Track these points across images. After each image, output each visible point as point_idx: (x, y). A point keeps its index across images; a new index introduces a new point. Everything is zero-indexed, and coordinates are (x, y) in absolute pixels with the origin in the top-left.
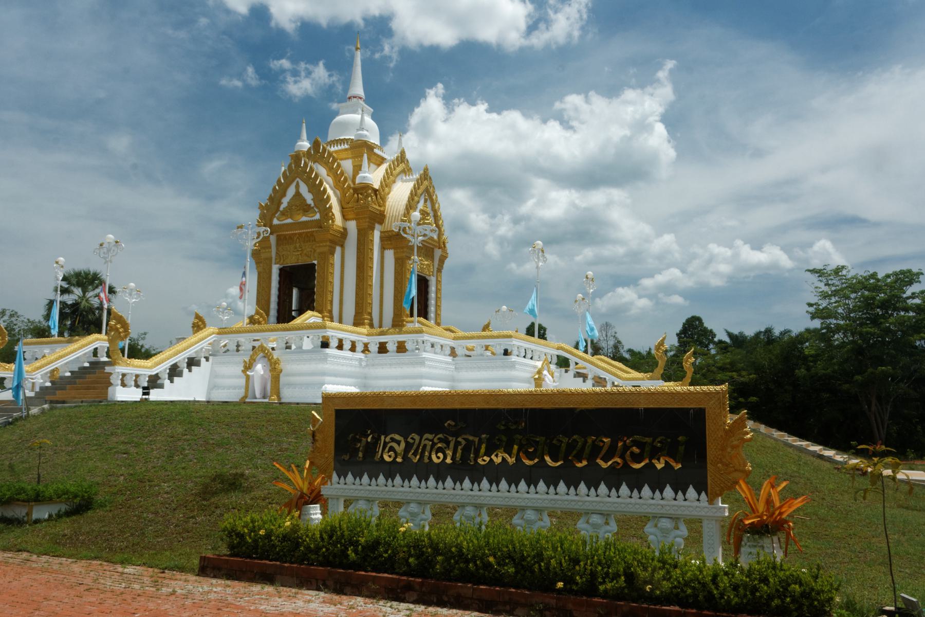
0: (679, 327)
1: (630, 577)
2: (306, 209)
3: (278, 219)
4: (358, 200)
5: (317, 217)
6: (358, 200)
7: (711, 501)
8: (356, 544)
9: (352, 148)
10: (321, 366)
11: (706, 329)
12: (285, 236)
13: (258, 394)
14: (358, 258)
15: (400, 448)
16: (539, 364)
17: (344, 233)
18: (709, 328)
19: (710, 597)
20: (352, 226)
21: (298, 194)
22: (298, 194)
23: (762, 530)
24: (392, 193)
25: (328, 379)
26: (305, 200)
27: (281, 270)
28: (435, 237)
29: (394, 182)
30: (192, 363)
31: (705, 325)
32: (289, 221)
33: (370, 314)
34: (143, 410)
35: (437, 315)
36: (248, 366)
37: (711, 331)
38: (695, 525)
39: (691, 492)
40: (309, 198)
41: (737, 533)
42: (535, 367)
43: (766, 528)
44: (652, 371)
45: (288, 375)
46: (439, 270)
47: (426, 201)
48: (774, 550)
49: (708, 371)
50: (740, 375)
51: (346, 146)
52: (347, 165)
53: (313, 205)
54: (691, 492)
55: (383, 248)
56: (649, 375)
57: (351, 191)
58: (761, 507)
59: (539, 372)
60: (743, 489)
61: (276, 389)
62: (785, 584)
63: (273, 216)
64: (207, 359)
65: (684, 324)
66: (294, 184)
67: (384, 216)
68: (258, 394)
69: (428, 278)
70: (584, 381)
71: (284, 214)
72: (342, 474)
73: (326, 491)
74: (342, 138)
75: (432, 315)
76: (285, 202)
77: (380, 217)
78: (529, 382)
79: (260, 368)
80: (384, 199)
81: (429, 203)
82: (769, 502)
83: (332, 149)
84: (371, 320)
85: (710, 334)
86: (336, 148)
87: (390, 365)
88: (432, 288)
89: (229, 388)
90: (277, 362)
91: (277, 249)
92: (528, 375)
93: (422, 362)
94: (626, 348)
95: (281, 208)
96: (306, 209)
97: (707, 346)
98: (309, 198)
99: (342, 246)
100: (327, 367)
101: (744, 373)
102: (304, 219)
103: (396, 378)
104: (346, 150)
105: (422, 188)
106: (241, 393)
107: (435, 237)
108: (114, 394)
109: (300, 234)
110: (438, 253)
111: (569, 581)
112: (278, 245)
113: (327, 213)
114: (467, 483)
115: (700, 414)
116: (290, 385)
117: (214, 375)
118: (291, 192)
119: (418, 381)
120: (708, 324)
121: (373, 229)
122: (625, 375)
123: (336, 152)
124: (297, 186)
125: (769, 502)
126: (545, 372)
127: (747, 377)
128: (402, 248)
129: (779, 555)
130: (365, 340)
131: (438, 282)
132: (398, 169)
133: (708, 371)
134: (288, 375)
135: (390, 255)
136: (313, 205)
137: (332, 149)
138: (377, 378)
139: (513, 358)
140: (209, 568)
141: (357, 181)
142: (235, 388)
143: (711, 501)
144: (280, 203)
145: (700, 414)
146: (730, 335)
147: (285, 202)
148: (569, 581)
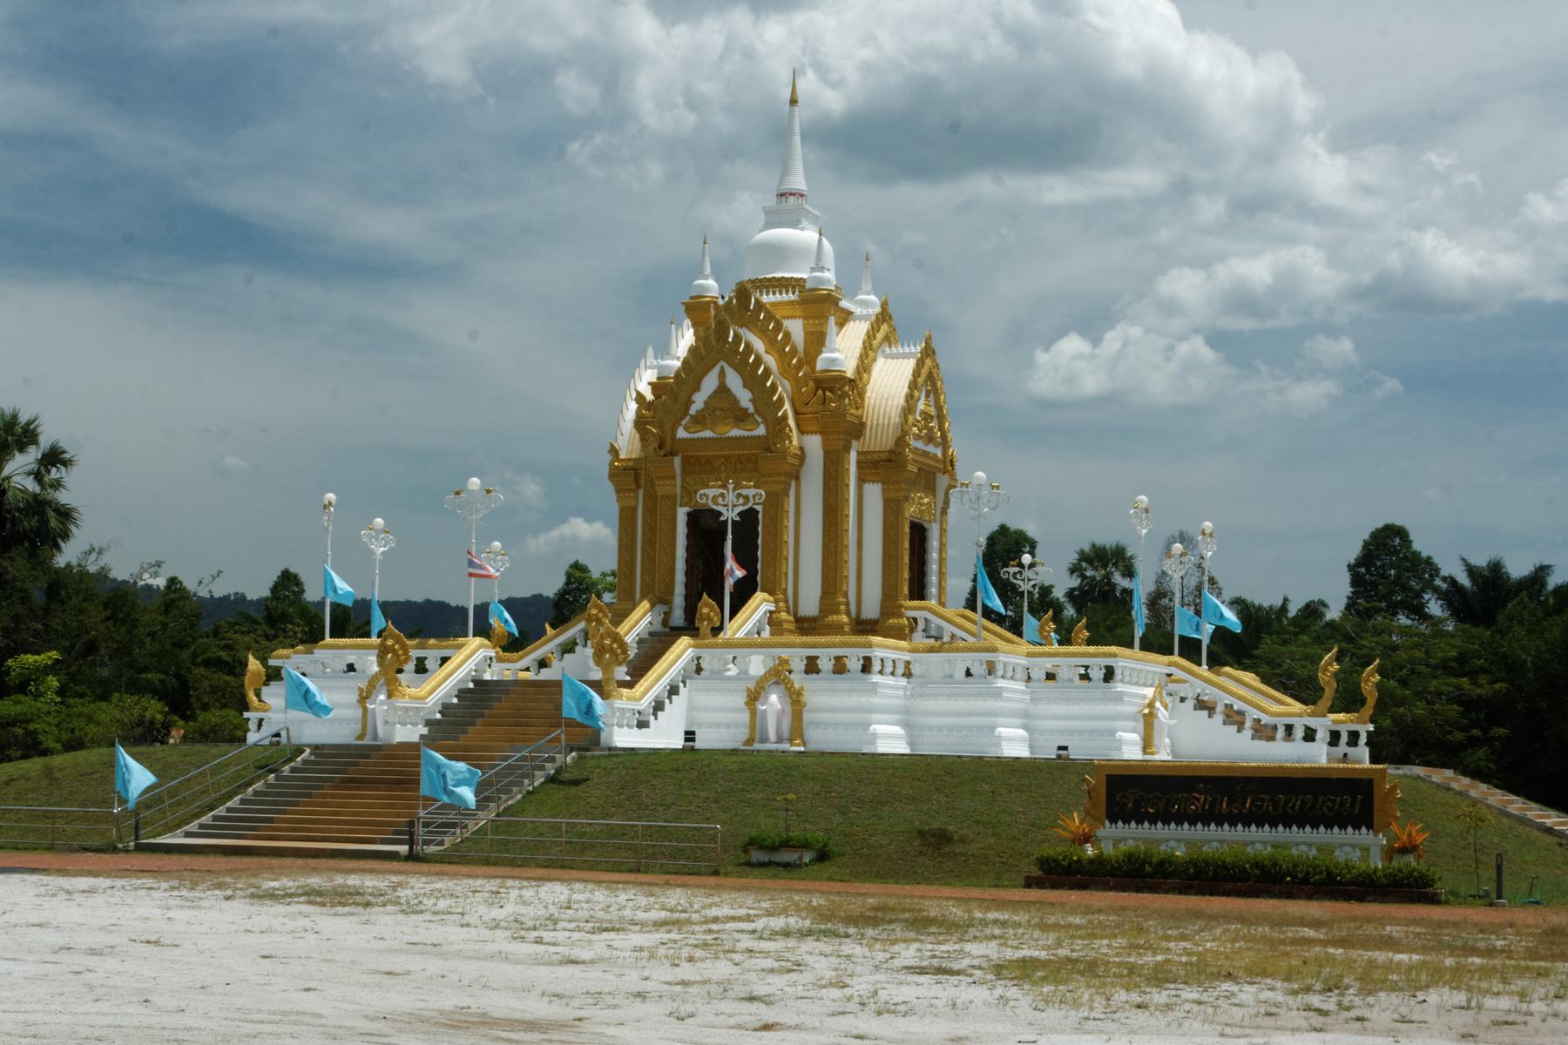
0: (1354, 551)
1: (1329, 873)
2: (741, 417)
3: (686, 429)
4: (824, 401)
5: (761, 430)
6: (824, 401)
7: (1376, 835)
8: (1150, 864)
9: (803, 302)
10: (864, 700)
11: (1416, 555)
12: (698, 459)
13: (772, 735)
14: (826, 500)
15: (1162, 804)
16: (1149, 692)
17: (802, 456)
18: (1424, 555)
19: (1372, 882)
20: (814, 443)
21: (723, 390)
22: (723, 390)
23: (1404, 850)
24: (872, 380)
25: (875, 717)
26: (736, 401)
27: (689, 514)
28: (940, 455)
29: (874, 360)
30: (673, 691)
31: (1416, 546)
32: (707, 434)
33: (846, 594)
34: (688, 757)
35: (941, 589)
36: (754, 697)
37: (1428, 561)
38: (1366, 850)
39: (1364, 830)
40: (744, 398)
41: (1390, 853)
42: (1144, 697)
43: (1404, 850)
44: (1314, 703)
45: (814, 710)
46: (944, 512)
47: (927, 396)
48: (1411, 859)
49: (1413, 671)
50: (1475, 683)
51: (791, 297)
52: (796, 328)
53: (751, 410)
54: (1364, 830)
55: (861, 480)
56: (1309, 709)
57: (811, 383)
58: (1405, 838)
59: (1151, 705)
60: (1394, 827)
61: (797, 730)
62: (1411, 873)
63: (677, 423)
64: (684, 683)
65: (1366, 545)
66: (716, 370)
67: (863, 425)
68: (772, 735)
69: (926, 525)
70: (1239, 731)
71: (700, 421)
72: (1113, 820)
73: (1100, 832)
74: (778, 275)
75: (933, 591)
76: (699, 401)
77: (858, 429)
78: (1135, 720)
79: (774, 701)
80: (861, 395)
81: (932, 398)
82: (1410, 835)
83: (767, 299)
84: (847, 604)
85: (1423, 567)
86: (778, 297)
87: (949, 695)
88: (933, 544)
89: (718, 726)
90: (799, 693)
91: (684, 480)
92: (1134, 709)
93: (998, 694)
94: (1229, 594)
95: (693, 410)
96: (741, 417)
97: (1419, 595)
98: (744, 398)
99: (797, 478)
100: (875, 700)
101: (1482, 679)
102: (736, 432)
103: (957, 714)
104: (792, 303)
105: (924, 372)
106: (744, 733)
107: (940, 455)
108: (611, 736)
109: (727, 458)
110: (942, 481)
111: (1294, 877)
112: (684, 472)
113: (778, 426)
114: (1213, 826)
115: (1370, 782)
116: (817, 725)
117: (691, 708)
118: (710, 383)
119: (992, 720)
120: (1422, 544)
121: (847, 449)
122: (1282, 709)
123: (774, 304)
124: (722, 374)
125: (1410, 835)
126: (1158, 704)
127: (1484, 688)
128: (898, 482)
129: (1414, 864)
130: (908, 657)
131: (943, 531)
132: (880, 336)
133: (1413, 671)
134: (814, 710)
135: (874, 492)
136: (751, 410)
137: (767, 299)
138: (926, 713)
139: (1119, 687)
140: (1030, 883)
141: (820, 366)
142: (728, 726)
143: (1376, 835)
144: (689, 402)
145: (1370, 782)
146: (1471, 571)
147: (699, 401)
148: (1294, 877)
